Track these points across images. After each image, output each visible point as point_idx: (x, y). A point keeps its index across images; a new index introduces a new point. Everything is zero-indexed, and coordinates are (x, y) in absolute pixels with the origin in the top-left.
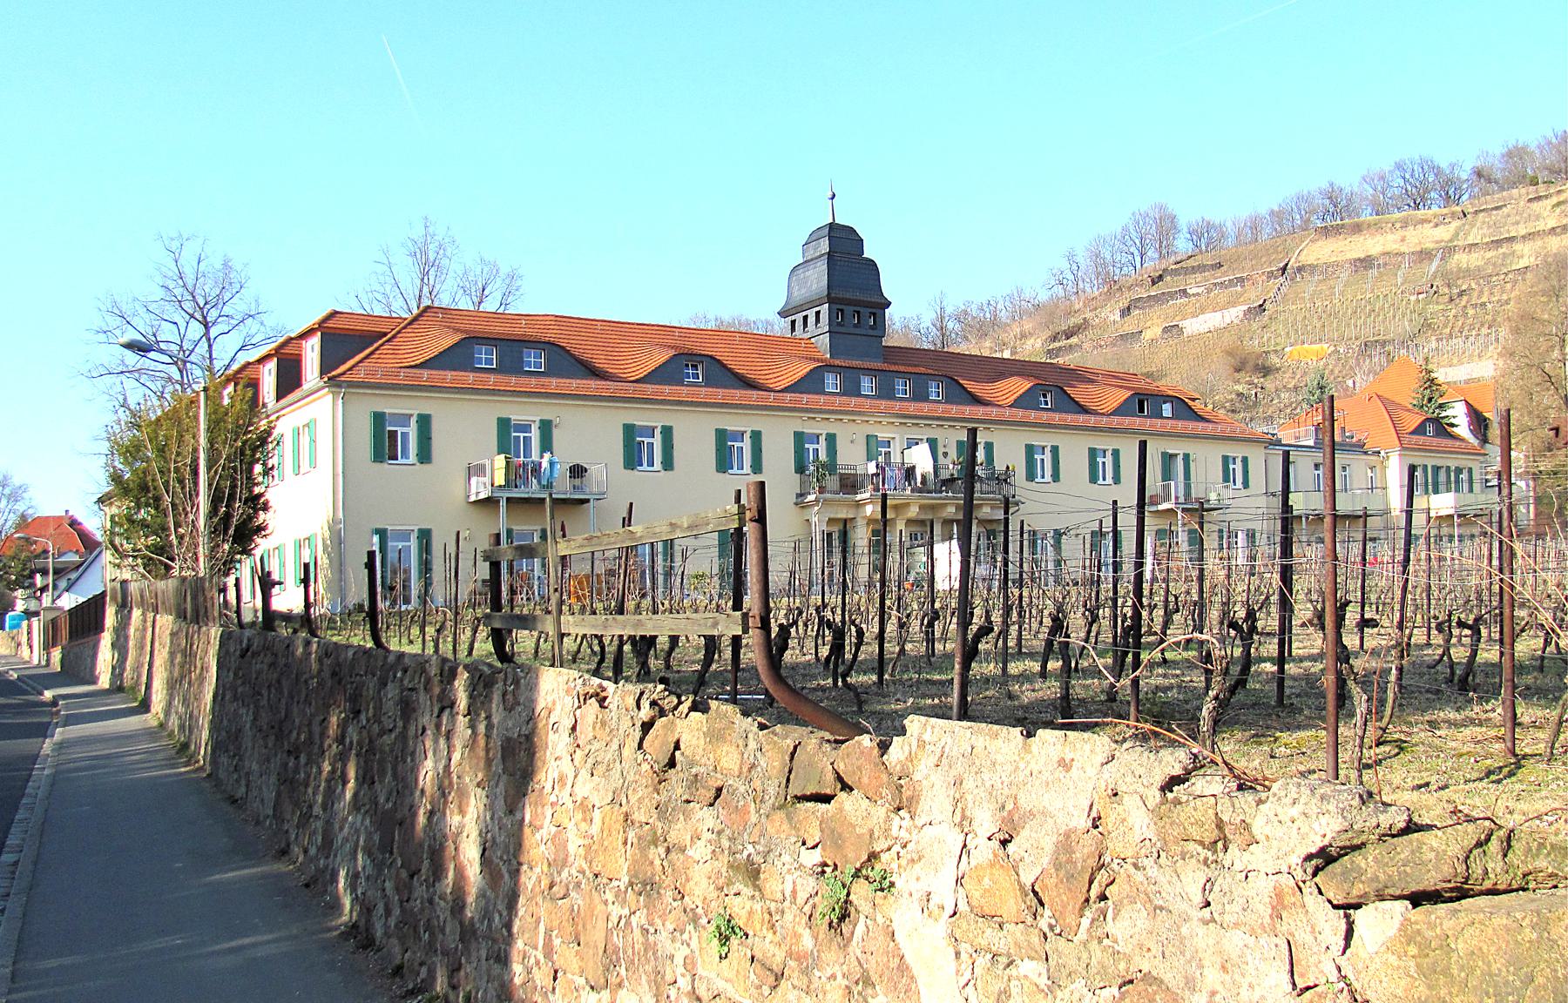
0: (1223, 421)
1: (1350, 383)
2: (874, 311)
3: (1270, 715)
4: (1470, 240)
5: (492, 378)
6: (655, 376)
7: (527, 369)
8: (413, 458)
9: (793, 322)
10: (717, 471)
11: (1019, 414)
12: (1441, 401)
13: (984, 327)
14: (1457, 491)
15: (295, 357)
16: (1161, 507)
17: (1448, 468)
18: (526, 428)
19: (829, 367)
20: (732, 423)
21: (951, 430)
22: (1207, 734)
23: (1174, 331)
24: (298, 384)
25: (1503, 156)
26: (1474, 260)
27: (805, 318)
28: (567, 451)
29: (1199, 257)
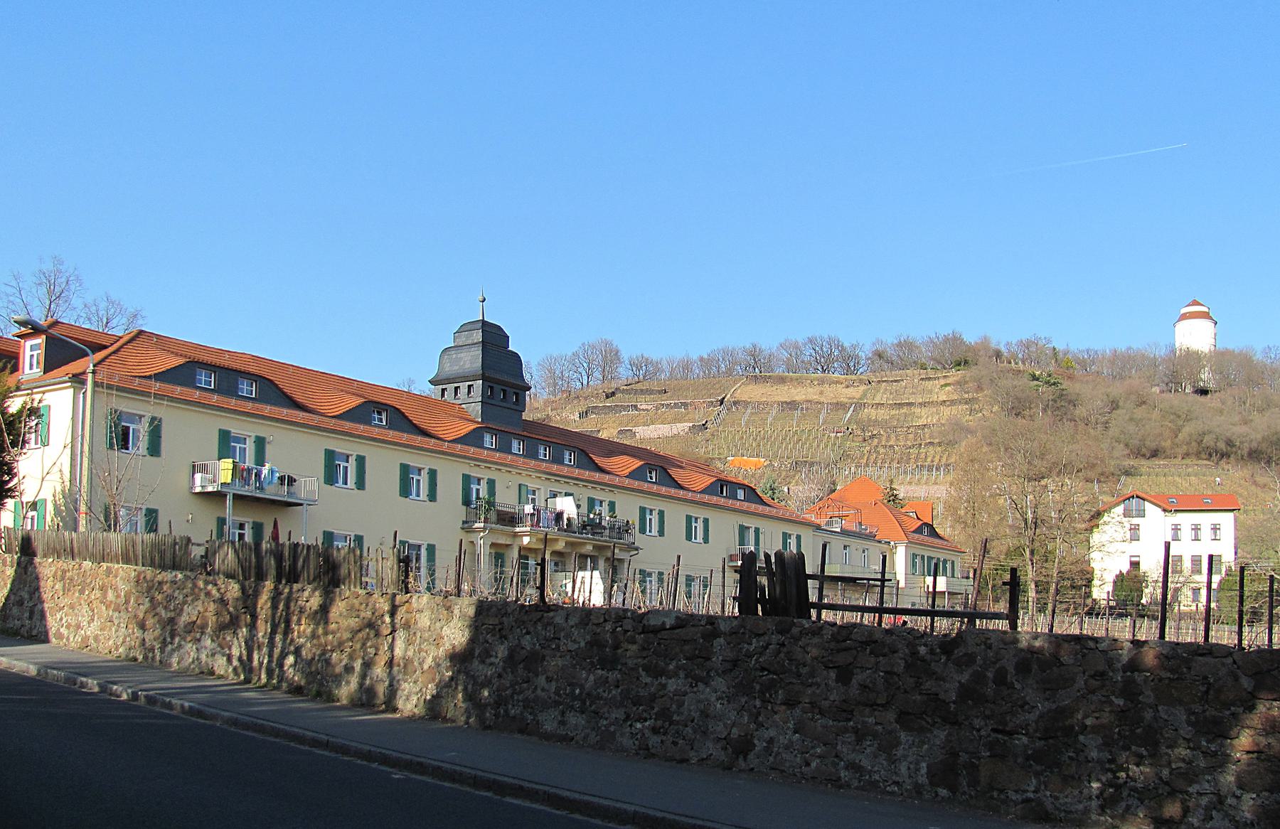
2: (504, 388)
5: (250, 404)
6: (348, 415)
7: (240, 394)
9: (443, 390)
10: (400, 495)
15: (14, 355)
20: (413, 460)
23: (628, 434)
26: (882, 414)
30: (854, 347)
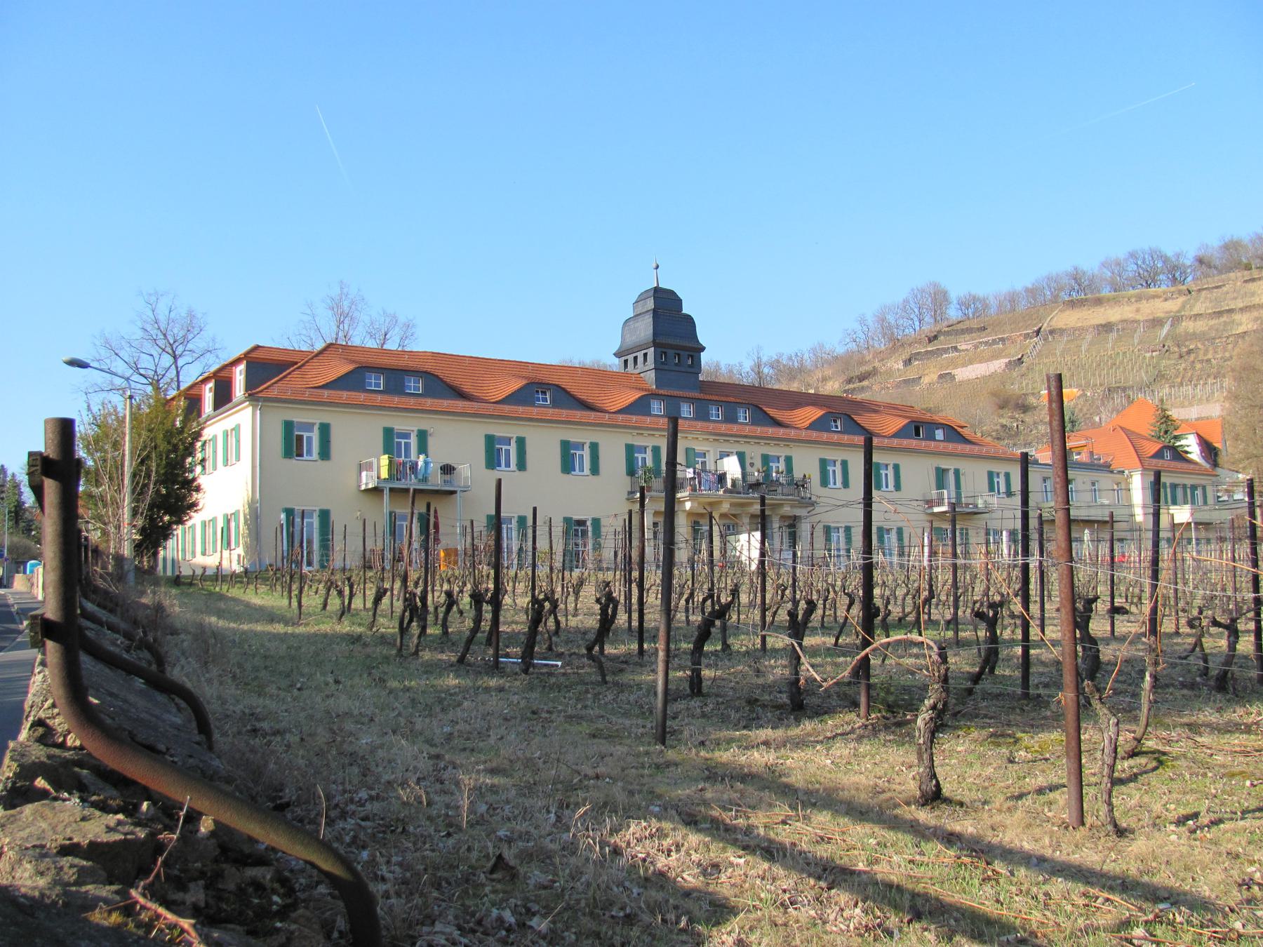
0: (988, 445)
1: (1097, 419)
3: (1013, 708)
4: (1195, 311)
5: (379, 397)
6: (513, 399)
8: (315, 455)
9: (626, 362)
11: (814, 435)
12: (1176, 433)
13: (792, 373)
14: (1193, 503)
16: (936, 510)
17: (1184, 486)
18: (407, 436)
19: (654, 395)
20: (574, 436)
21: (756, 446)
22: (923, 747)
23: (948, 377)
24: (230, 400)
25: (1221, 247)
26: (1200, 326)
27: (636, 358)
28: (440, 452)
29: (968, 322)
30: (1178, 255)
